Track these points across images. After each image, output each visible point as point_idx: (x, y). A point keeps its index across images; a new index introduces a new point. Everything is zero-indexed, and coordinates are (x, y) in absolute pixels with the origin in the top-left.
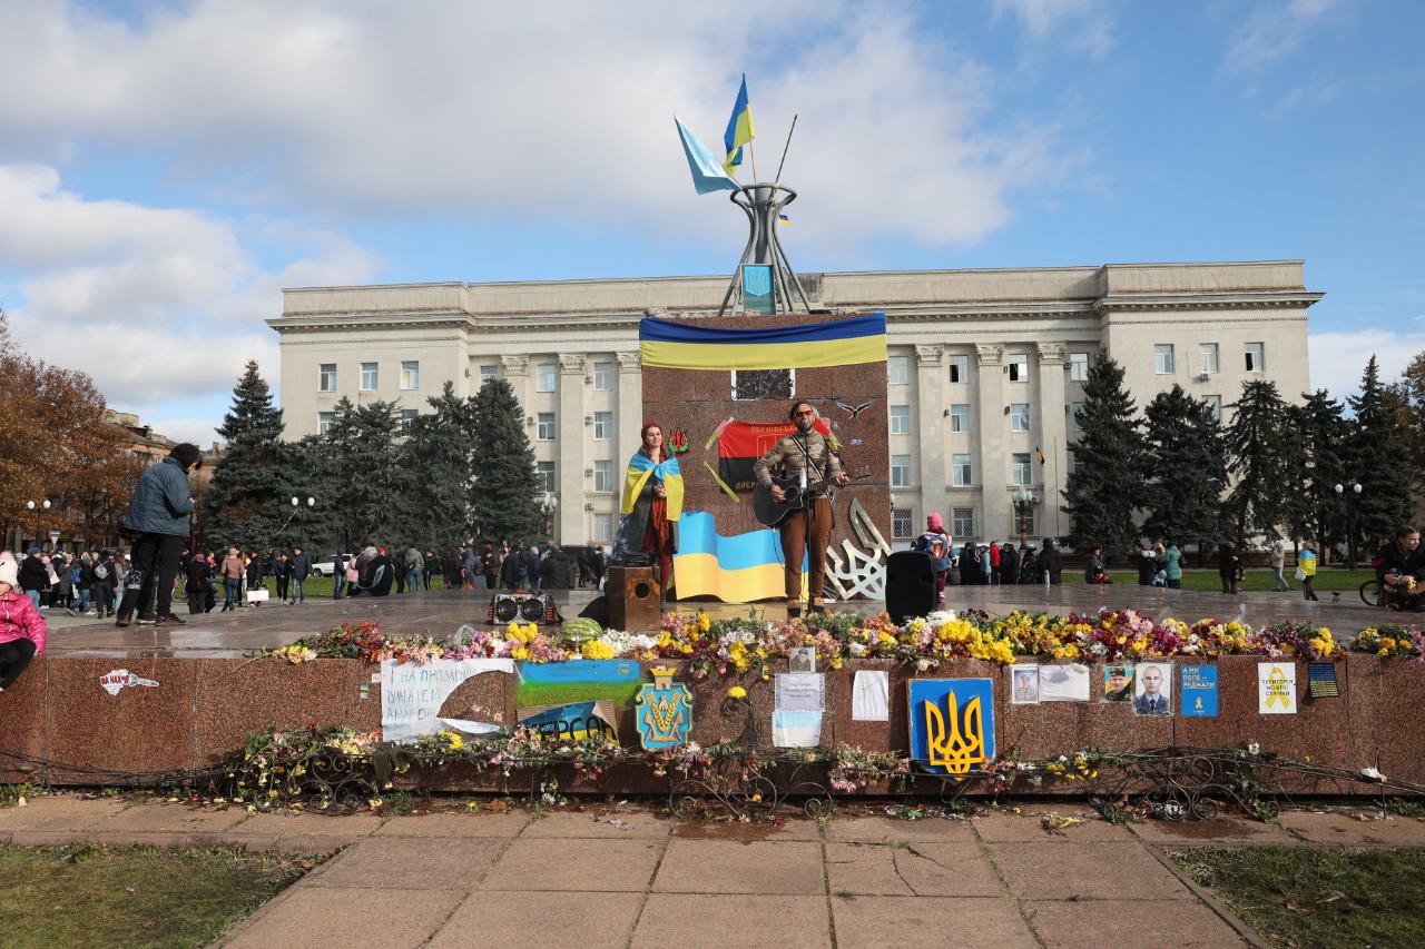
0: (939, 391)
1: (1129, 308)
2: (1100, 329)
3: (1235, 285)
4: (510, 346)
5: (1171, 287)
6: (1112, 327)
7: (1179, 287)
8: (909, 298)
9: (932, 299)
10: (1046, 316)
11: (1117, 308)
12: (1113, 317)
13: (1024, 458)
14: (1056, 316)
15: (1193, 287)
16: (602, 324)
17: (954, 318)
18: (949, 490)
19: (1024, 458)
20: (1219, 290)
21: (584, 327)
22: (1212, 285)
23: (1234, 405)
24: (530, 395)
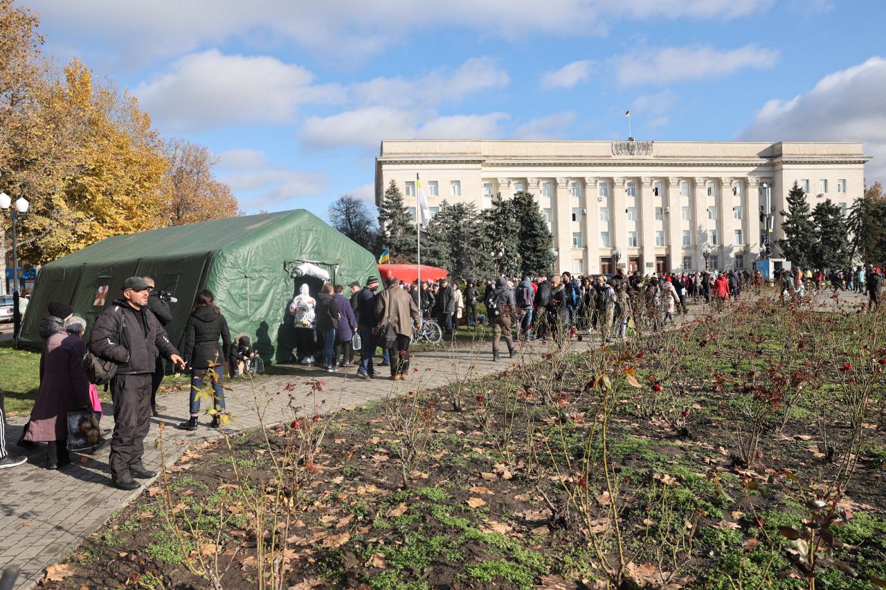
0: (568, 201)
1: (792, 163)
2: (774, 171)
3: (835, 153)
4: (531, 174)
5: (808, 153)
6: (783, 171)
7: (812, 153)
8: (690, 155)
9: (701, 155)
10: (752, 165)
11: (787, 163)
12: (785, 166)
13: (739, 232)
14: (756, 165)
15: (817, 153)
16: (454, 161)
17: (712, 165)
18: (600, 249)
19: (739, 232)
20: (829, 155)
21: (540, 165)
22: (825, 152)
23: (851, 208)
24: (542, 202)
